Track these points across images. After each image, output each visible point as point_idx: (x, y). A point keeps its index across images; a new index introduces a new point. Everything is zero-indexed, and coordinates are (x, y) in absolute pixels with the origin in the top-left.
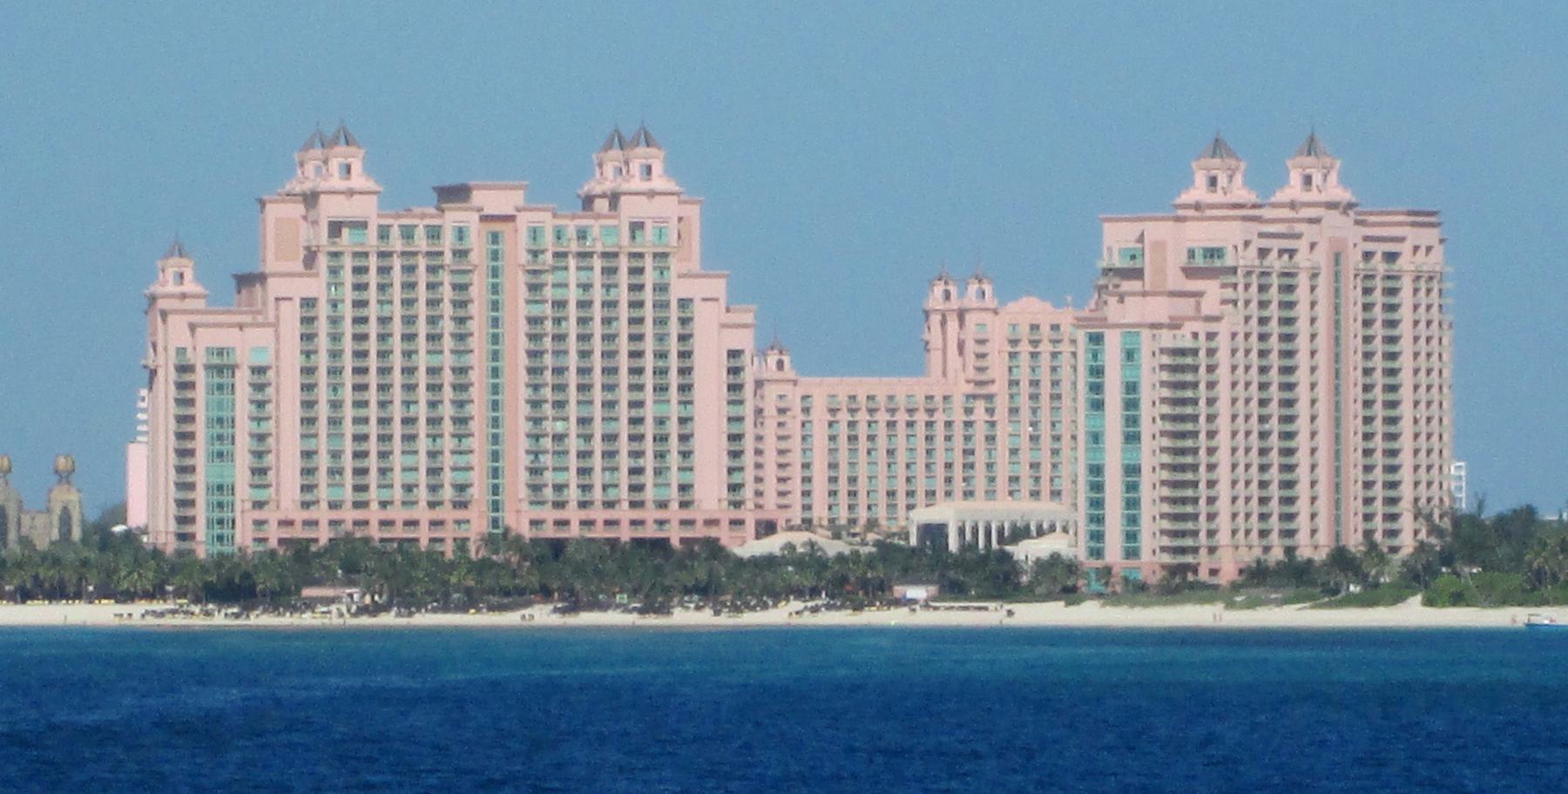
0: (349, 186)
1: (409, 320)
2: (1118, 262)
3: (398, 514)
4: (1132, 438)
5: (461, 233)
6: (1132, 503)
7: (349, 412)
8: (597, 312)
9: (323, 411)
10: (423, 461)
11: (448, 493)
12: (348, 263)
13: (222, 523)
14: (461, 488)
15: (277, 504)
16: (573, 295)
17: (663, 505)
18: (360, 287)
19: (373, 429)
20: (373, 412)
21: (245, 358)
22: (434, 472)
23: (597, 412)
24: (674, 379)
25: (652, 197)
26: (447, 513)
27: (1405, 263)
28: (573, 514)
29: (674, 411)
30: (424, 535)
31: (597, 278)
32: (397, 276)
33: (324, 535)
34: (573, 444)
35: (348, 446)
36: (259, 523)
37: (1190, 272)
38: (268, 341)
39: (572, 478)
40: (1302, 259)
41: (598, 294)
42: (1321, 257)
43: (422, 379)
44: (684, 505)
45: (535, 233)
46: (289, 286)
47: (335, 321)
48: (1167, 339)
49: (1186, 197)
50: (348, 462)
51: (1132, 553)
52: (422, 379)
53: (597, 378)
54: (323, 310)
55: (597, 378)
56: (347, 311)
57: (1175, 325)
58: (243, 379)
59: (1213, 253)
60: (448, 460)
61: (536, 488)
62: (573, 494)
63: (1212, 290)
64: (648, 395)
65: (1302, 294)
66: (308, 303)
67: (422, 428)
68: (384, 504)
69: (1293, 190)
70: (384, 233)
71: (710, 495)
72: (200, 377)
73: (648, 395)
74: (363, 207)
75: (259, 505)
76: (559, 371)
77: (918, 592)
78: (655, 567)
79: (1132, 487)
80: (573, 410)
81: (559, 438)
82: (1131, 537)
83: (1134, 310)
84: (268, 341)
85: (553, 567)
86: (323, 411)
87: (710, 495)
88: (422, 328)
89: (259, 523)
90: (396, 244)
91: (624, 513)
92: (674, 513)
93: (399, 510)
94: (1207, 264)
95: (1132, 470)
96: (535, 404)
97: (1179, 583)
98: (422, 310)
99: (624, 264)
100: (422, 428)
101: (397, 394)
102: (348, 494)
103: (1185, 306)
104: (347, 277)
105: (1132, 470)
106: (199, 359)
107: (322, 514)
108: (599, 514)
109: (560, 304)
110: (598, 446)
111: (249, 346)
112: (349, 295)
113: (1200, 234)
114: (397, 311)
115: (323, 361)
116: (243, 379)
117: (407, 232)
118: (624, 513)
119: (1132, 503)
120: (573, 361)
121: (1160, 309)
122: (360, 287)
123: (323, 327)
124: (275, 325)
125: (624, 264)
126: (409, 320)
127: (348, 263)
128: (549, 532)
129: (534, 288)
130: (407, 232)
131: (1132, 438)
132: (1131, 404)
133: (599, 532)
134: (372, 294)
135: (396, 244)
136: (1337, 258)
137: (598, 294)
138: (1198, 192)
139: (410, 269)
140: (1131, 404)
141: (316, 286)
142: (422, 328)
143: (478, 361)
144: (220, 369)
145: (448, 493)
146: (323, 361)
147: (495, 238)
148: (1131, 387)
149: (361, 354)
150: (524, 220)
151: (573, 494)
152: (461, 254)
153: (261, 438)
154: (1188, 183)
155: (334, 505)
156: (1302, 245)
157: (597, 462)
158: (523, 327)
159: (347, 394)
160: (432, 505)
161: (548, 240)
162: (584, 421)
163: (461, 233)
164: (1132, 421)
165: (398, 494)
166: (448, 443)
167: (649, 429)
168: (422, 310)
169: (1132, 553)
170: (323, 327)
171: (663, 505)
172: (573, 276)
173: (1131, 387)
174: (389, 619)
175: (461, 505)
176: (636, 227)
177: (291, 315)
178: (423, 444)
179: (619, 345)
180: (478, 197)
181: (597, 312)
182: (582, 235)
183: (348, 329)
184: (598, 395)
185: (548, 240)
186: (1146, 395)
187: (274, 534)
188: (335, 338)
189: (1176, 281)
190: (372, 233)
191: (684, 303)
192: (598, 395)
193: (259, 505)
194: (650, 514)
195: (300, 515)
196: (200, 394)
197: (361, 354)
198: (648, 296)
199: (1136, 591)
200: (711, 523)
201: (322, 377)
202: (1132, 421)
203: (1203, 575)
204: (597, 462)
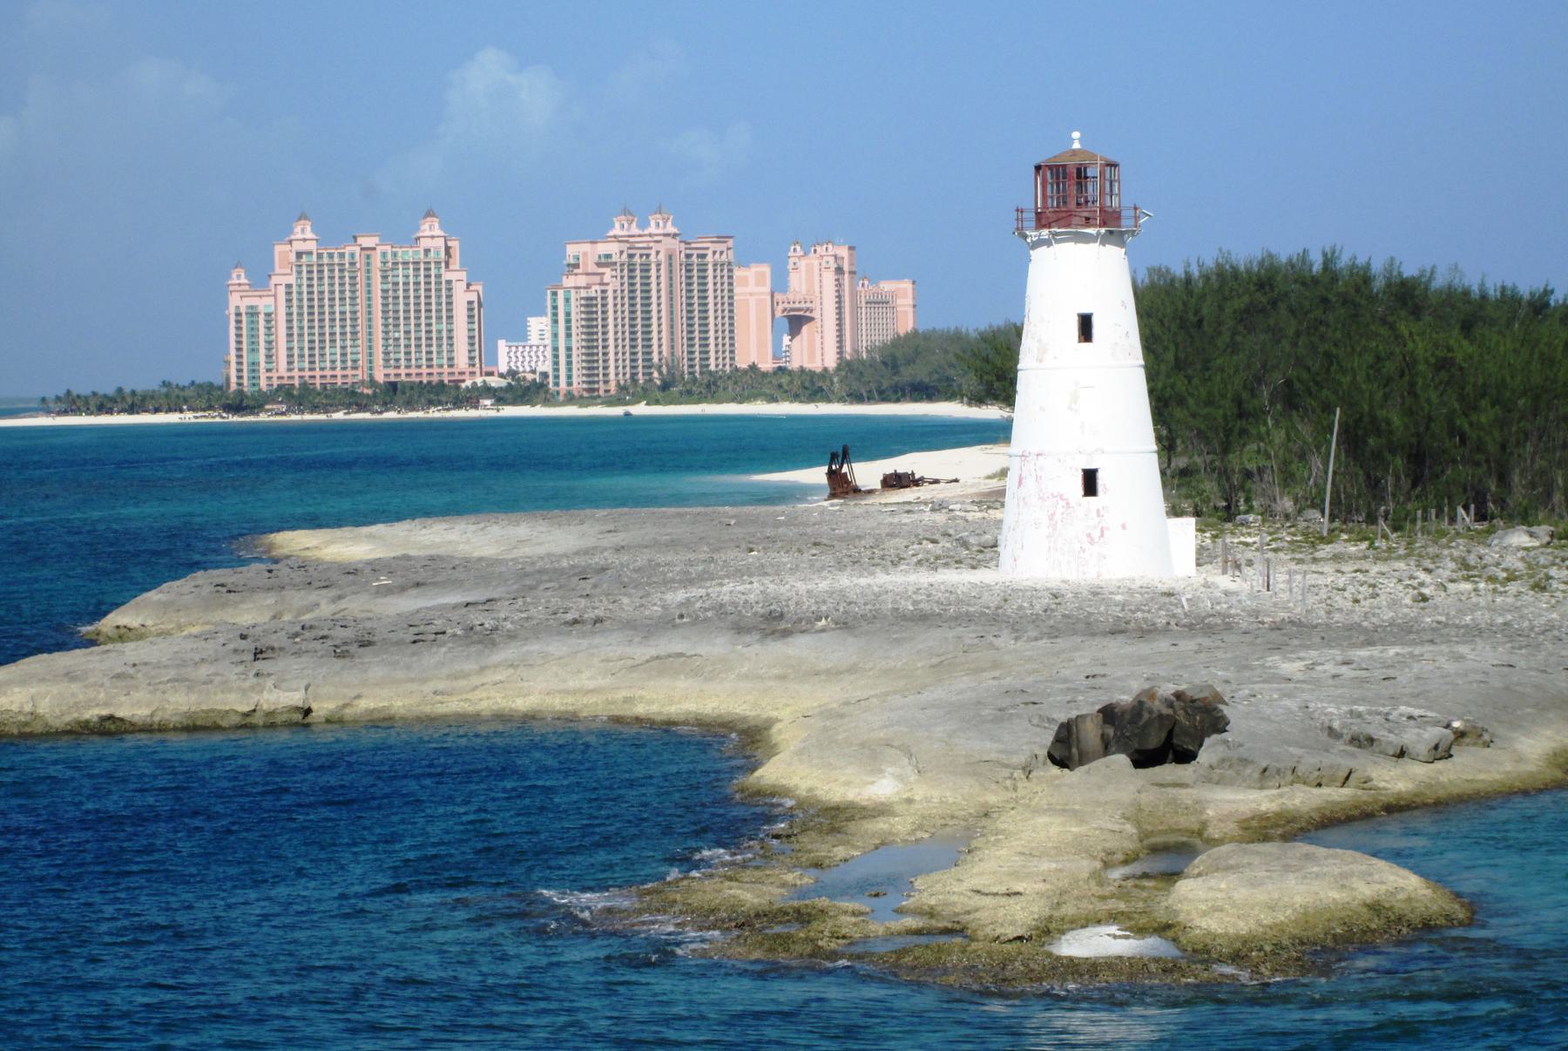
0: (304, 235)
1: (332, 292)
2: (572, 261)
3: (328, 373)
4: (569, 335)
5: (352, 255)
6: (569, 363)
7: (306, 331)
8: (412, 287)
9: (296, 331)
10: (338, 351)
11: (349, 364)
12: (304, 269)
13: (254, 377)
14: (355, 361)
15: (281, 369)
16: (401, 280)
17: (419, 367)
18: (310, 279)
19: (316, 338)
20: (316, 331)
21: (262, 309)
22: (344, 355)
23: (412, 328)
24: (444, 313)
25: (432, 234)
26: (349, 372)
27: (709, 258)
28: (403, 371)
29: (444, 326)
30: (339, 381)
31: (411, 272)
32: (326, 274)
33: (339, 381)
34: (402, 342)
35: (306, 345)
36: (269, 378)
37: (599, 265)
38: (271, 302)
39: (402, 356)
40: (653, 258)
41: (411, 280)
42: (662, 257)
43: (338, 316)
44: (451, 366)
45: (384, 254)
46: (284, 277)
47: (300, 293)
48: (583, 293)
49: (611, 233)
50: (306, 352)
51: (570, 384)
52: (338, 316)
53: (412, 314)
54: (295, 289)
55: (412, 314)
56: (305, 289)
57: (588, 287)
58: (262, 318)
59: (608, 256)
60: (349, 350)
61: (386, 361)
62: (403, 362)
63: (607, 271)
64: (434, 321)
65: (653, 273)
66: (289, 286)
67: (338, 337)
68: (322, 369)
69: (652, 229)
70: (320, 256)
71: (462, 361)
72: (244, 318)
73: (434, 321)
74: (311, 246)
75: (269, 370)
76: (397, 311)
77: (488, 402)
78: (209, 395)
79: (569, 356)
80: (402, 328)
81: (397, 339)
82: (569, 377)
83: (569, 282)
84: (271, 302)
85: (392, 393)
86: (296, 331)
87: (462, 361)
88: (337, 295)
89: (269, 378)
90: (326, 260)
91: (424, 370)
92: (446, 369)
93: (331, 370)
94: (605, 261)
95: (569, 349)
96: (386, 325)
97: (591, 396)
98: (337, 288)
99: (422, 266)
100: (338, 337)
101: (327, 323)
102: (306, 365)
103: (597, 279)
104: (304, 274)
105: (569, 349)
106: (243, 310)
107: (296, 373)
108: (413, 371)
109: (397, 284)
110: (413, 342)
111: (264, 304)
112: (305, 282)
113: (603, 248)
114: (326, 288)
115: (295, 310)
116: (262, 318)
117: (331, 256)
118: (338, 372)
119: (569, 363)
120: (401, 307)
121: (582, 281)
122: (310, 279)
123: (295, 296)
124: (275, 296)
125: (422, 266)
126: (332, 292)
127: (304, 269)
128: (392, 379)
129: (385, 277)
130: (331, 256)
131: (569, 335)
132: (568, 321)
133: (414, 379)
134: (315, 282)
135: (326, 260)
136: (670, 257)
137: (411, 280)
138: (617, 231)
139: (332, 271)
140: (568, 321)
141: (292, 280)
142: (337, 295)
143: (361, 309)
144: (252, 315)
145: (349, 364)
146: (295, 310)
147: (368, 257)
148: (568, 314)
149: (311, 307)
150: (379, 249)
151: (403, 362)
152: (353, 264)
153: (270, 342)
154: (612, 227)
155: (322, 369)
156: (653, 252)
157: (413, 349)
158: (380, 293)
159: (306, 324)
160: (344, 369)
161: (389, 257)
162: (407, 332)
163: (352, 255)
164: (568, 328)
165: (328, 364)
166: (349, 343)
167: (434, 335)
168: (337, 288)
169: (570, 384)
170: (295, 296)
171: (441, 366)
172: (400, 272)
173: (568, 314)
174: (294, 417)
175: (355, 368)
176: (427, 251)
177: (282, 291)
178: (338, 343)
179: (420, 298)
180: (360, 240)
181: (412, 287)
182: (395, 255)
183: (305, 296)
184: (413, 321)
185: (389, 257)
186: (573, 317)
187: (276, 382)
188: (301, 300)
189: (592, 268)
190: (314, 257)
191: (449, 282)
192: (413, 321)
193: (269, 370)
194: (435, 370)
195: (286, 374)
196: (244, 325)
197: (311, 307)
198: (433, 279)
199: (571, 399)
200: (462, 373)
201: (295, 317)
202: (568, 328)
203: (602, 393)
204: (413, 349)
